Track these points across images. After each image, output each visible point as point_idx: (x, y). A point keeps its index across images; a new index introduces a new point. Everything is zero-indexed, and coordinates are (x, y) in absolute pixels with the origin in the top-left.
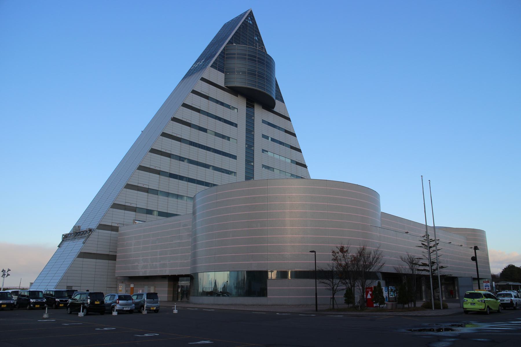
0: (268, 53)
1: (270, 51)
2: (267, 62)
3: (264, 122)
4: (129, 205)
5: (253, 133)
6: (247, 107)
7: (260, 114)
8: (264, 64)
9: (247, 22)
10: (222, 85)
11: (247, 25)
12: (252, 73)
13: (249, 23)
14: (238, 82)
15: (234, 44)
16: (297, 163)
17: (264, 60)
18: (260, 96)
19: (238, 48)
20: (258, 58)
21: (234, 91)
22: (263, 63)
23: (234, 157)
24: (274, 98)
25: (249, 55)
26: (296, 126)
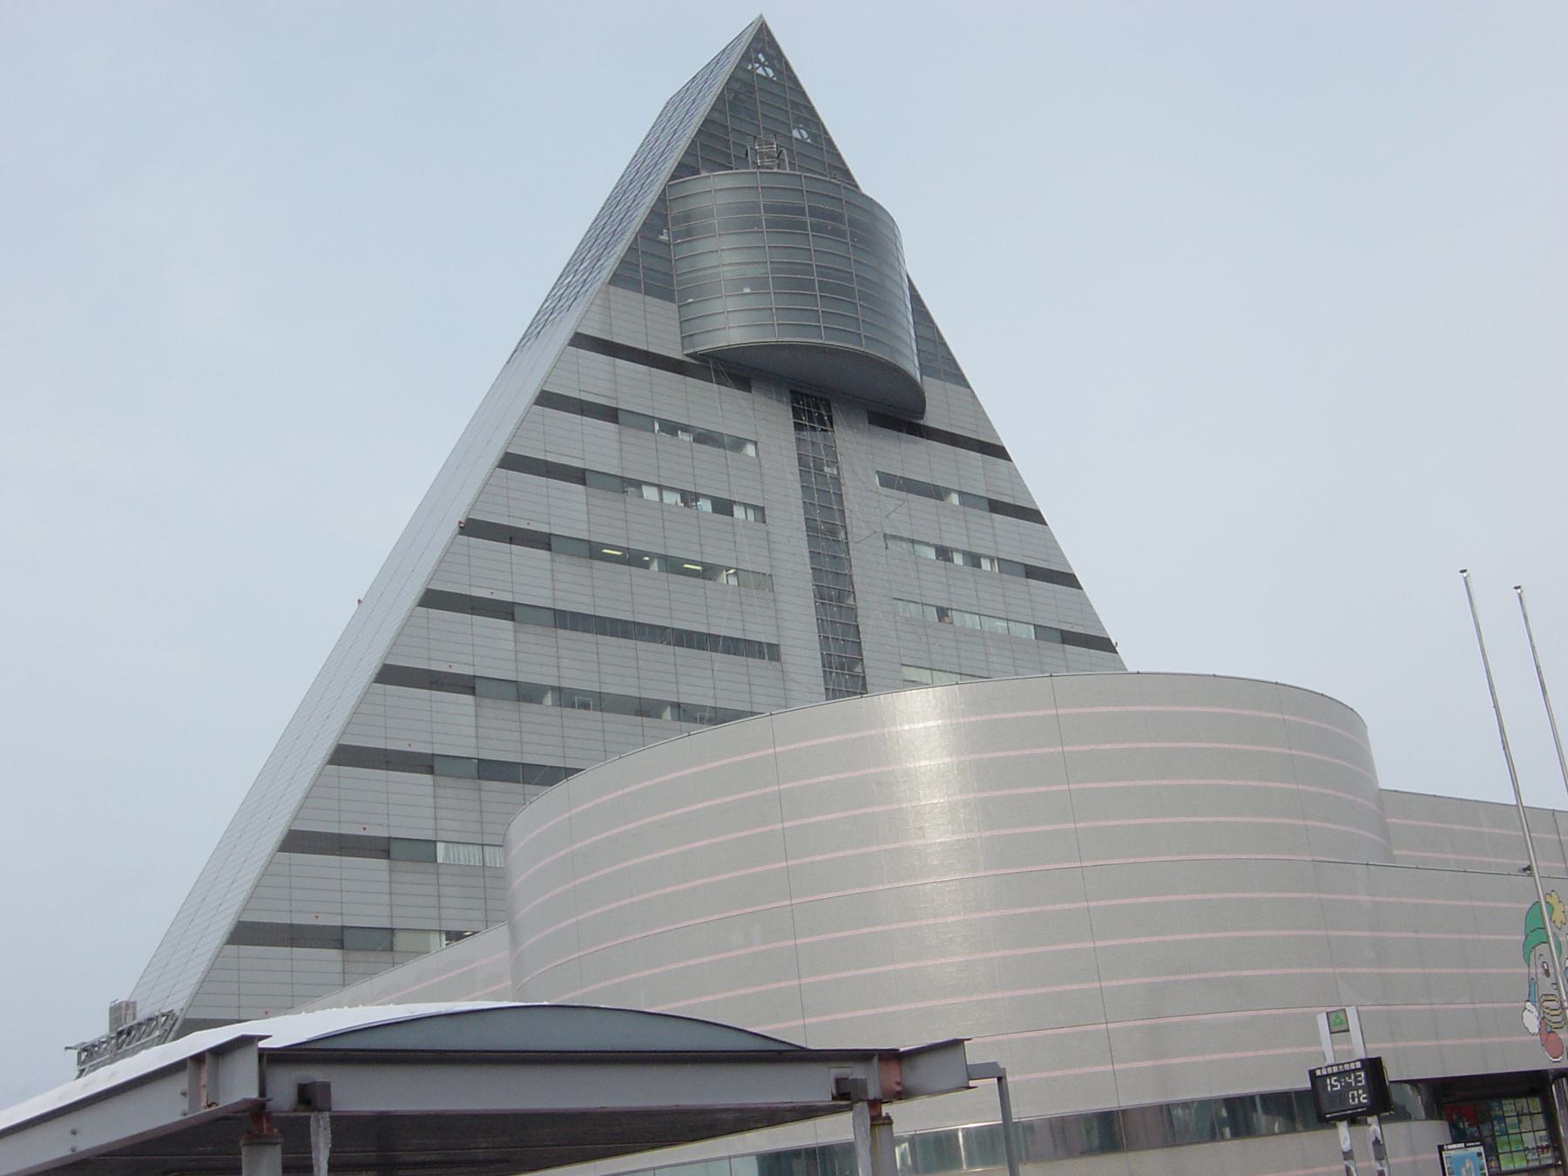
0: (865, 191)
1: (869, 183)
2: (852, 223)
3: (888, 481)
4: (443, 668)
5: (851, 601)
6: (799, 427)
7: (861, 453)
8: (837, 232)
9: (752, 72)
10: (677, 354)
11: (751, 90)
12: (793, 282)
13: (766, 78)
14: (732, 326)
15: (704, 174)
16: (1032, 572)
17: (837, 218)
18: (857, 382)
19: (717, 191)
20: (814, 212)
21: (734, 369)
22: (831, 223)
23: (770, 652)
24: (912, 366)
25: (768, 209)
26: (1038, 471)
